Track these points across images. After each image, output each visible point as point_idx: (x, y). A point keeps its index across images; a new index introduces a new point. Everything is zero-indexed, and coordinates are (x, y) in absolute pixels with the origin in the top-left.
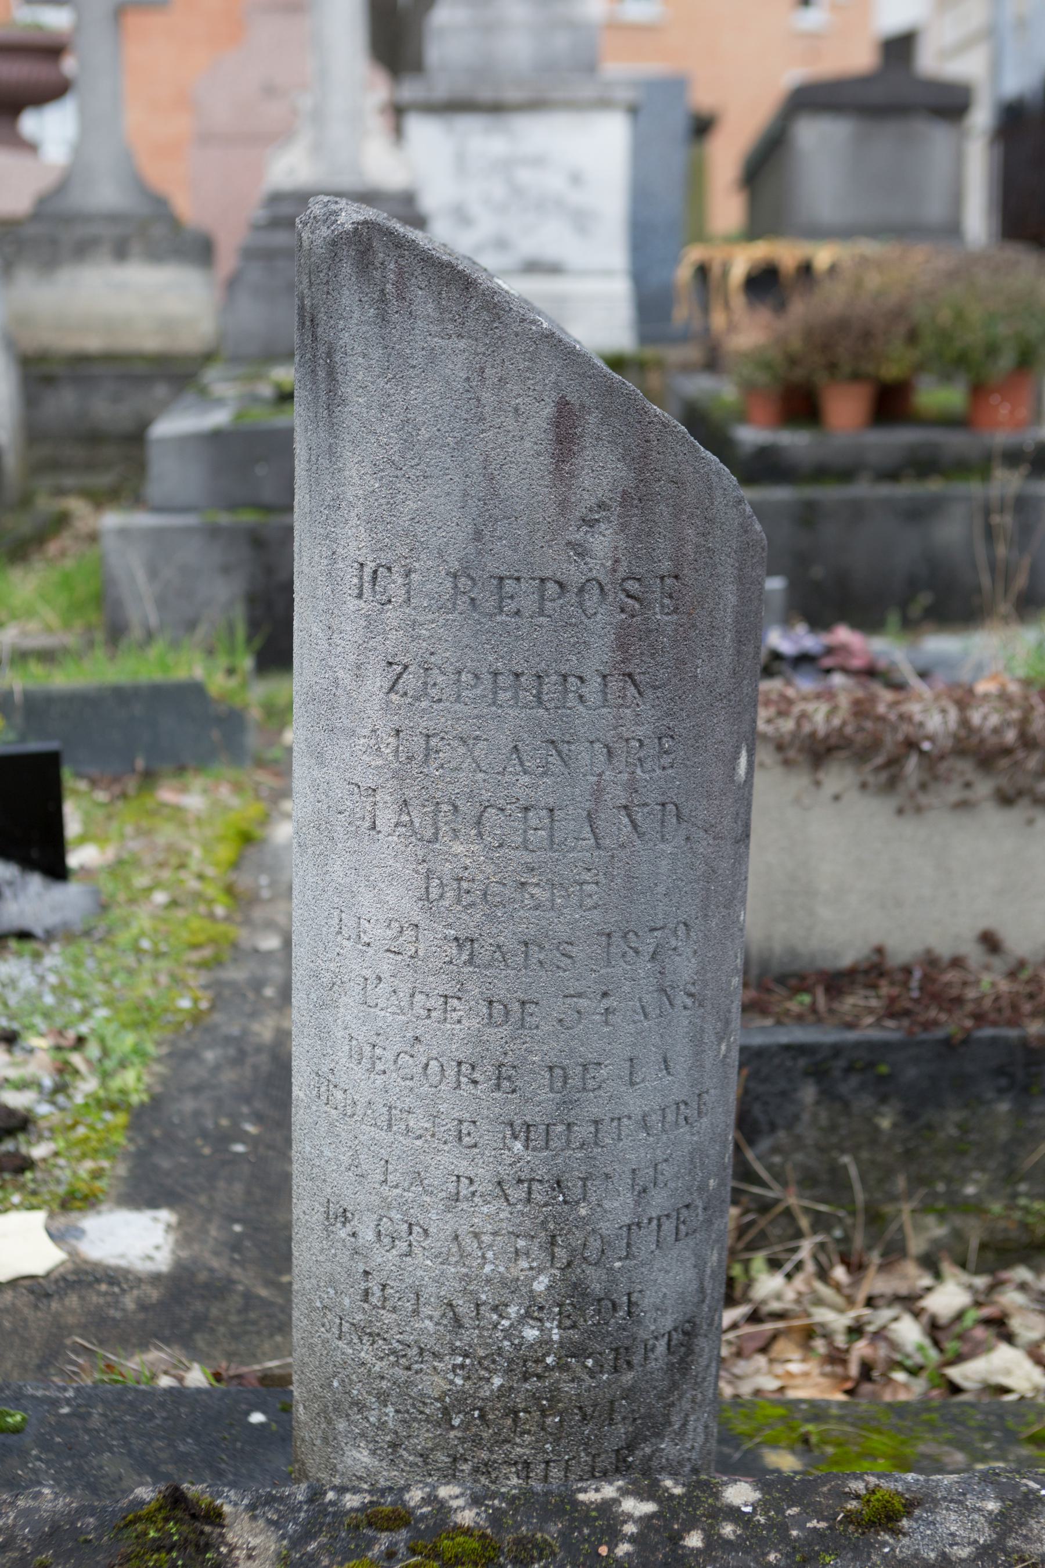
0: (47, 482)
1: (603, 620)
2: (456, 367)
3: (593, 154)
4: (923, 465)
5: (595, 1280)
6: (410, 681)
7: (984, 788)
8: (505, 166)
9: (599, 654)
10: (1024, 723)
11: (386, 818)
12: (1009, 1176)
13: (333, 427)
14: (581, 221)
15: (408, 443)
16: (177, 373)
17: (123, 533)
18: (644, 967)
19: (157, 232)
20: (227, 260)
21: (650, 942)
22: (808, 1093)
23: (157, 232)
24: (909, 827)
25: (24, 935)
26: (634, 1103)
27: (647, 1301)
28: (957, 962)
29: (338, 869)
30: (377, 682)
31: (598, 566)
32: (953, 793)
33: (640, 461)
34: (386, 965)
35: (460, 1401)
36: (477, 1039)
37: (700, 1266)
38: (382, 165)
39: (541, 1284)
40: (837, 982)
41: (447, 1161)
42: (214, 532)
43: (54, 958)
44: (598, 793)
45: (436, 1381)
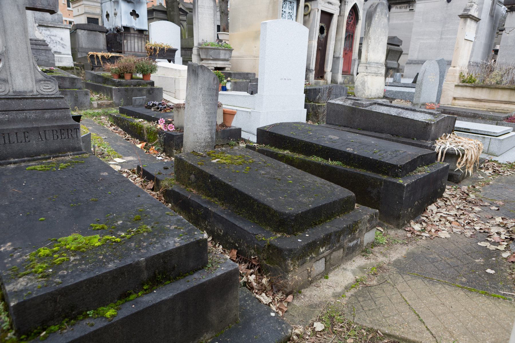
2: (208, 75)
14: (63, 46)
30: (201, 95)
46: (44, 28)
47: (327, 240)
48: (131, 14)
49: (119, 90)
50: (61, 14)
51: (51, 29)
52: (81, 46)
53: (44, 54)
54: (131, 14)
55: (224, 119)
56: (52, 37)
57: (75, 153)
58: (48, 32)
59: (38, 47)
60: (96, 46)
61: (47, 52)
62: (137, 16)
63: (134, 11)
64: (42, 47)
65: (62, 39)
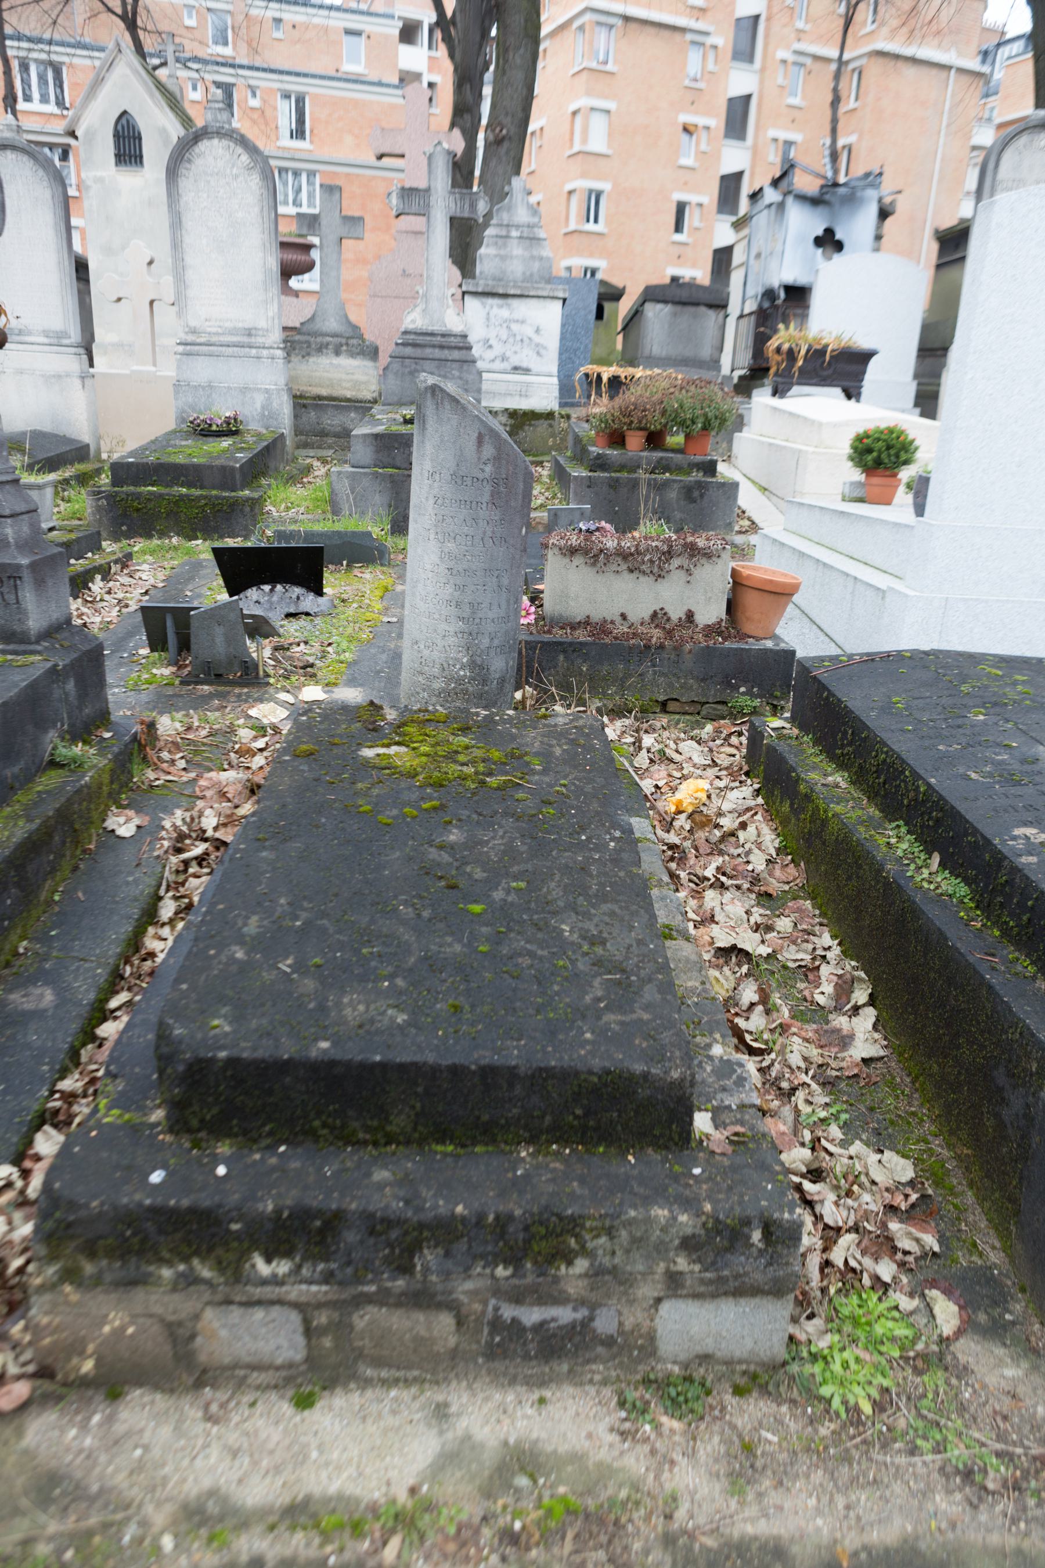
0: (304, 452)
1: (488, 489)
2: (454, 423)
3: (546, 318)
4: (663, 467)
5: (479, 661)
6: (440, 502)
7: (624, 566)
8: (507, 323)
9: (486, 497)
10: (637, 546)
11: (432, 537)
12: (622, 687)
13: (423, 435)
14: (539, 351)
15: (442, 441)
16: (362, 407)
17: (339, 473)
18: (495, 579)
19: (353, 343)
20: (384, 359)
21: (496, 573)
22: (561, 657)
23: (353, 343)
24: (600, 577)
25: (307, 614)
26: (491, 615)
27: (492, 669)
28: (612, 622)
29: (419, 551)
30: (432, 501)
31: (487, 475)
32: (614, 567)
33: (498, 449)
34: (430, 575)
35: (444, 690)
36: (452, 595)
37: (507, 663)
38: (452, 322)
39: (465, 660)
40: (574, 626)
41: (443, 626)
42: (376, 475)
43: (318, 620)
44: (485, 533)
45: (438, 685)
46: (496, 301)
47: (304, 1234)
48: (819, 242)
49: (590, 483)
50: (548, 259)
51: (515, 303)
52: (646, 352)
53: (456, 373)
54: (819, 242)
55: (732, 607)
56: (515, 327)
57: (11, 647)
58: (505, 313)
59: (446, 354)
60: (688, 353)
61: (465, 367)
62: (839, 246)
63: (829, 232)
64: (456, 354)
65: (538, 331)
